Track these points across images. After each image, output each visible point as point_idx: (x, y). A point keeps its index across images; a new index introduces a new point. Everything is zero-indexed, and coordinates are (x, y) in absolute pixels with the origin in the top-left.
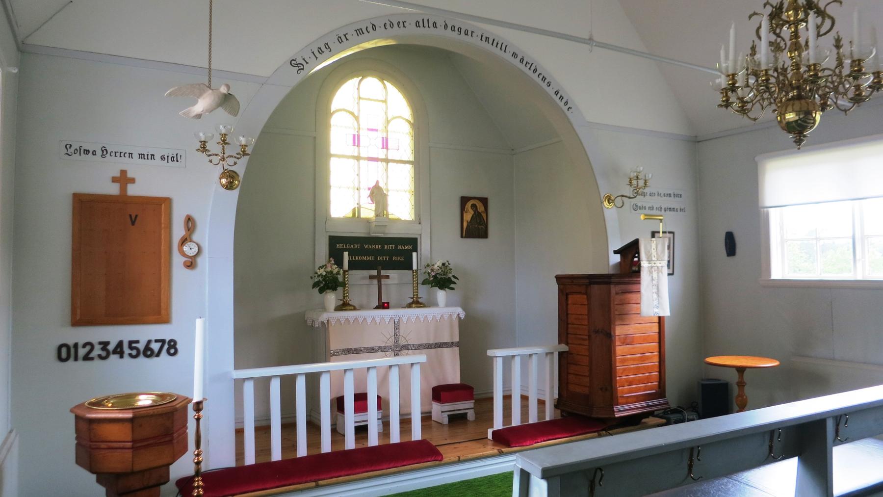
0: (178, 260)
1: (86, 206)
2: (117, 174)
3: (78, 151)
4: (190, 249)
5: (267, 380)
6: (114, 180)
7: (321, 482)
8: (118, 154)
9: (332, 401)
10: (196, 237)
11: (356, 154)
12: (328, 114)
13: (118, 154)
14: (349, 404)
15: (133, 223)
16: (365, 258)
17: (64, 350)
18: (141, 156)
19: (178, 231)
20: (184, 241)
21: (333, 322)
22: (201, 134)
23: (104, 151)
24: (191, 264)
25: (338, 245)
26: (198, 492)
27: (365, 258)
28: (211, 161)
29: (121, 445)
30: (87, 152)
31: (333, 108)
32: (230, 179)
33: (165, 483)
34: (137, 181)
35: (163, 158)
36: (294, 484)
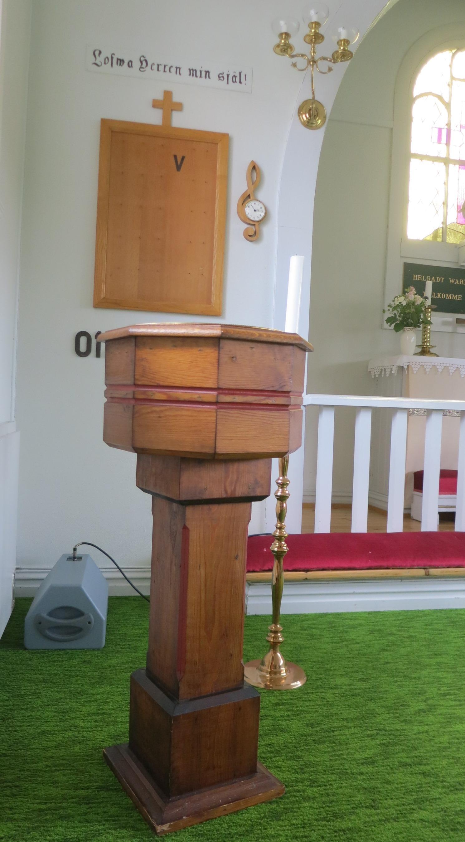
0: (236, 227)
1: (119, 141)
2: (160, 96)
3: (109, 60)
4: (253, 211)
5: (354, 411)
6: (156, 104)
7: (433, 571)
8: (161, 68)
9: (407, 476)
10: (261, 195)
11: (443, 155)
12: (410, 100)
13: (161, 68)
14: (432, 481)
15: (179, 168)
16: (449, 297)
17: (83, 340)
18: (193, 72)
19: (238, 185)
20: (247, 198)
21: (415, 369)
22: (282, 23)
23: (144, 62)
24: (253, 233)
25: (413, 275)
26: (280, 547)
27: (449, 297)
28: (294, 65)
29: (109, 570)
30: (121, 62)
31: (417, 90)
32: (311, 112)
33: (260, 498)
34: (185, 107)
35: (220, 77)
36: (394, 568)
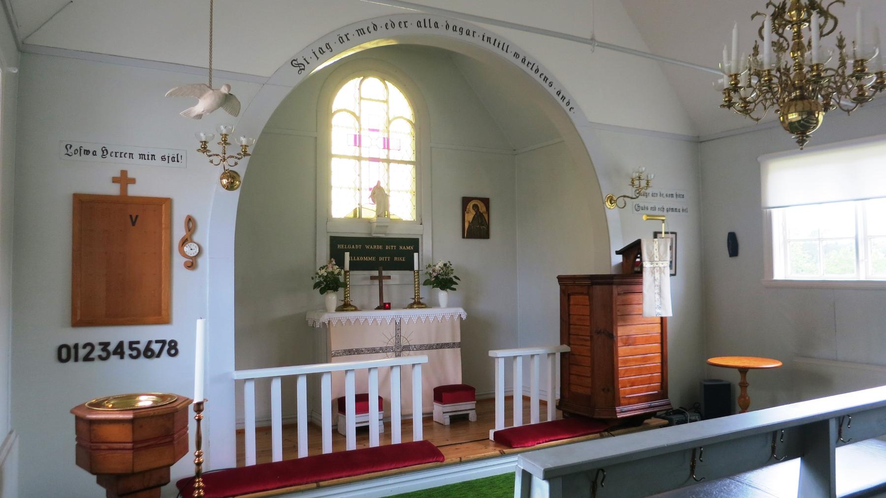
0: (178, 261)
1: (86, 207)
2: (118, 174)
3: (78, 151)
4: (191, 250)
5: (268, 381)
6: (115, 180)
7: (322, 483)
8: (118, 155)
9: (333, 402)
10: (196, 237)
11: (357, 155)
12: (329, 114)
13: (118, 155)
14: (351, 405)
15: (134, 224)
16: (366, 259)
17: (64, 351)
18: (142, 156)
19: (179, 232)
20: (184, 242)
21: (334, 323)
22: (202, 134)
23: (105, 151)
24: (191, 265)
25: (339, 245)
26: (199, 493)
27: (366, 259)
28: (211, 162)
29: (122, 445)
30: (87, 152)
31: (334, 108)
32: (231, 179)
33: (165, 484)
34: (137, 181)
35: (163, 158)
36: (295, 485)
